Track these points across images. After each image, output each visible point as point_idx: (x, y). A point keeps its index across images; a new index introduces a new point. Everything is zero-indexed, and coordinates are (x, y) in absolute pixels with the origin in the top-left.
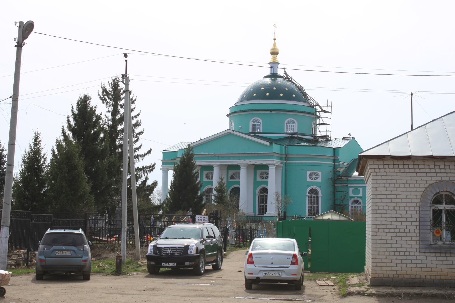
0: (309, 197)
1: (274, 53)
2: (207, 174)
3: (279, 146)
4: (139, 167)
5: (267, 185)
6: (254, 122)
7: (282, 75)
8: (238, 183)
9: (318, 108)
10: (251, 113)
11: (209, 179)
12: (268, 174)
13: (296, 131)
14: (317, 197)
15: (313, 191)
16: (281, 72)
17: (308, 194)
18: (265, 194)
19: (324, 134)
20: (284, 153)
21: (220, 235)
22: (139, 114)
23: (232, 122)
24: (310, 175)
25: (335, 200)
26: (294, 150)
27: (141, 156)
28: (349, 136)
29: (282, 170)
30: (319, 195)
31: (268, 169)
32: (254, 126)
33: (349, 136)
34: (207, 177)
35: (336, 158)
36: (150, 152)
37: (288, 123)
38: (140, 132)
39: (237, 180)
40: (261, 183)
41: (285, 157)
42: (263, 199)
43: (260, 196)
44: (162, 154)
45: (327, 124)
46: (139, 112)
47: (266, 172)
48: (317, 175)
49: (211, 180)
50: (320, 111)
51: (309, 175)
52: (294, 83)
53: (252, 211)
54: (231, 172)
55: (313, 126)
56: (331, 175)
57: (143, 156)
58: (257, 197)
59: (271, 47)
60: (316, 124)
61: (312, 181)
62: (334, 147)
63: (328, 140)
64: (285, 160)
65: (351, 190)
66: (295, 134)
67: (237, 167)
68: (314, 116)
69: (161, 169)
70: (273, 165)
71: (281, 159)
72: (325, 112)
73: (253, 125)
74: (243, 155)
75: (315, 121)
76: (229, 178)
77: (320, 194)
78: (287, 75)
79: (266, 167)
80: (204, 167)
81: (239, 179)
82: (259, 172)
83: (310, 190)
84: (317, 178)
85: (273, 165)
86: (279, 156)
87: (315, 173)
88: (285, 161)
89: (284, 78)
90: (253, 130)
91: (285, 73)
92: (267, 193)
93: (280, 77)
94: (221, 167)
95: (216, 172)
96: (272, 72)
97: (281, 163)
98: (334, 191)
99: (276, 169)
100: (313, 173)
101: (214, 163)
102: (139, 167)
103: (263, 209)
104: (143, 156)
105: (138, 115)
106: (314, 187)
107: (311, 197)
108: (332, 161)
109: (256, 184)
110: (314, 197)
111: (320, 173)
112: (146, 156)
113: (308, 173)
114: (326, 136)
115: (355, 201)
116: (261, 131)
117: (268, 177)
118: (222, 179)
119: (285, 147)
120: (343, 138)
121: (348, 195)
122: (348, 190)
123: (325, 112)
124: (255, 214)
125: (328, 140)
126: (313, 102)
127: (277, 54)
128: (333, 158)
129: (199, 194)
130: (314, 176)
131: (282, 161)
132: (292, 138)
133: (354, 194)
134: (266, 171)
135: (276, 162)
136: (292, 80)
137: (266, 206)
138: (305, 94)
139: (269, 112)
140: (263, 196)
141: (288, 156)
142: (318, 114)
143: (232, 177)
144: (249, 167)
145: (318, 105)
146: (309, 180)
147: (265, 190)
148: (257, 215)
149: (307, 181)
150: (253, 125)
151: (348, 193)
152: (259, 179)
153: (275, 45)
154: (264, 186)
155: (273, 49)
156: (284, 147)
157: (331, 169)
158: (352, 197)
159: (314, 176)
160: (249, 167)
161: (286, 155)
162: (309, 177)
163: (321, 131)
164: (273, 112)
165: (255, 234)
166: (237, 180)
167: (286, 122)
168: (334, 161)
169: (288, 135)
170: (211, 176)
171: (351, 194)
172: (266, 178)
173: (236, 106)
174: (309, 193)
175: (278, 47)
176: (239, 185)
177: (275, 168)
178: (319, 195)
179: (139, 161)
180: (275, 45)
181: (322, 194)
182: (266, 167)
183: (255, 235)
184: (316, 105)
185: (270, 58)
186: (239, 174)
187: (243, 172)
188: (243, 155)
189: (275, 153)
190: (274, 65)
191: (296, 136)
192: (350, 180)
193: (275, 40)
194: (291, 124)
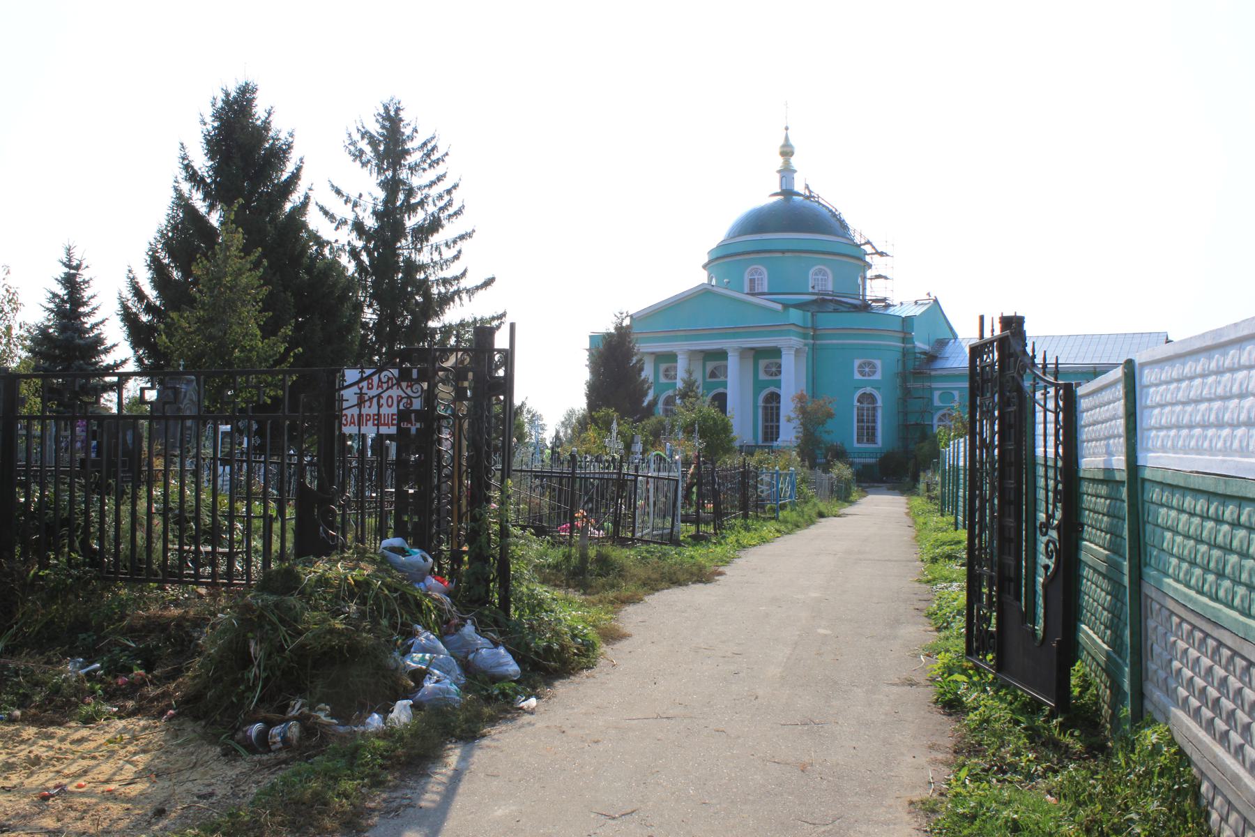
0: (858, 409)
1: (787, 152)
2: (767, 366)
3: (801, 312)
4: (464, 320)
5: (780, 388)
6: (752, 275)
7: (802, 192)
8: (725, 385)
9: (868, 249)
10: (747, 257)
11: (671, 379)
12: (780, 366)
13: (830, 287)
14: (874, 409)
15: (868, 398)
16: (799, 187)
17: (856, 403)
18: (774, 404)
19: (881, 295)
20: (810, 325)
21: (1021, 382)
22: (458, 185)
23: (712, 277)
24: (860, 366)
25: (906, 414)
26: (829, 320)
27: (468, 291)
28: (928, 297)
29: (807, 358)
30: (878, 405)
31: (781, 357)
32: (752, 281)
33: (928, 297)
34: (666, 376)
35: (908, 336)
36: (489, 282)
37: (816, 274)
38: (464, 233)
39: (722, 379)
40: (768, 383)
41: (812, 333)
42: (772, 414)
43: (765, 408)
44: (588, 339)
45: (886, 278)
46: (456, 181)
47: (776, 363)
48: (874, 366)
49: (674, 381)
50: (872, 254)
51: (875, 372)
52: (824, 206)
53: (752, 438)
54: (710, 365)
55: (860, 281)
56: (900, 369)
57: (471, 292)
58: (760, 411)
59: (782, 142)
60: (864, 278)
61: (770, 378)
62: (903, 316)
63: (888, 306)
64: (813, 339)
65: (937, 394)
66: (828, 295)
67: (721, 355)
68: (862, 264)
69: (586, 366)
70: (790, 347)
71: (805, 336)
72: (882, 254)
73: (751, 279)
74: (732, 331)
75: (864, 272)
76: (708, 375)
77: (879, 403)
78: (810, 192)
79: (776, 352)
80: (660, 358)
81: (726, 377)
82: (762, 363)
83: (860, 397)
84: (874, 373)
85: (790, 347)
86: (800, 330)
87: (870, 363)
88: (812, 341)
89: (808, 198)
90: (751, 290)
91: (807, 187)
92: (779, 402)
93: (798, 194)
94: (692, 354)
95: (681, 364)
96: (784, 188)
97: (806, 345)
98: (906, 394)
99: (795, 356)
100: (865, 363)
101: (680, 348)
102: (464, 320)
103: (771, 432)
104: (471, 292)
105: (455, 187)
106: (869, 390)
107: (863, 409)
108: (901, 340)
109: (758, 386)
110: (868, 409)
111: (878, 363)
112: (481, 292)
113: (857, 363)
114: (884, 300)
115: (944, 415)
116: (766, 291)
117: (780, 372)
118: (690, 373)
119: (813, 315)
120: (916, 302)
121: (932, 403)
122: (932, 394)
123: (882, 254)
124: (757, 442)
125: (888, 306)
126: (859, 237)
127: (792, 154)
128: (901, 335)
129: (645, 404)
130: (867, 370)
131: (806, 341)
132: (824, 300)
133: (942, 402)
134: (777, 360)
135: (796, 341)
136: (820, 200)
137: (778, 427)
138: (844, 226)
139: (780, 255)
140: (772, 408)
141: (818, 332)
142: (868, 259)
143: (713, 375)
144: (744, 352)
145: (868, 243)
146: (857, 376)
147: (774, 398)
148: (760, 443)
149: (661, 381)
150: (751, 279)
151: (931, 399)
152: (762, 376)
153: (787, 138)
154: (773, 389)
155: (784, 146)
156: (809, 314)
157: (899, 356)
158: (940, 408)
159: (867, 370)
160: (744, 352)
161: (815, 329)
162: (859, 371)
163: (874, 290)
164: (787, 255)
165: (759, 485)
166: (722, 379)
167: (811, 272)
168: (904, 340)
169: (814, 297)
170: (673, 373)
171: (937, 402)
172: (776, 375)
173: (721, 246)
174: (859, 401)
175: (792, 141)
176: (726, 388)
177: (793, 353)
178: (878, 405)
179: (462, 305)
180: (787, 138)
181: (883, 402)
182: (776, 352)
183: (759, 490)
184: (866, 243)
185: (779, 161)
186: (726, 367)
187: (733, 363)
188: (732, 331)
189: (794, 324)
190: (787, 172)
191: (831, 298)
192: (935, 377)
193: (787, 129)
194: (820, 277)
